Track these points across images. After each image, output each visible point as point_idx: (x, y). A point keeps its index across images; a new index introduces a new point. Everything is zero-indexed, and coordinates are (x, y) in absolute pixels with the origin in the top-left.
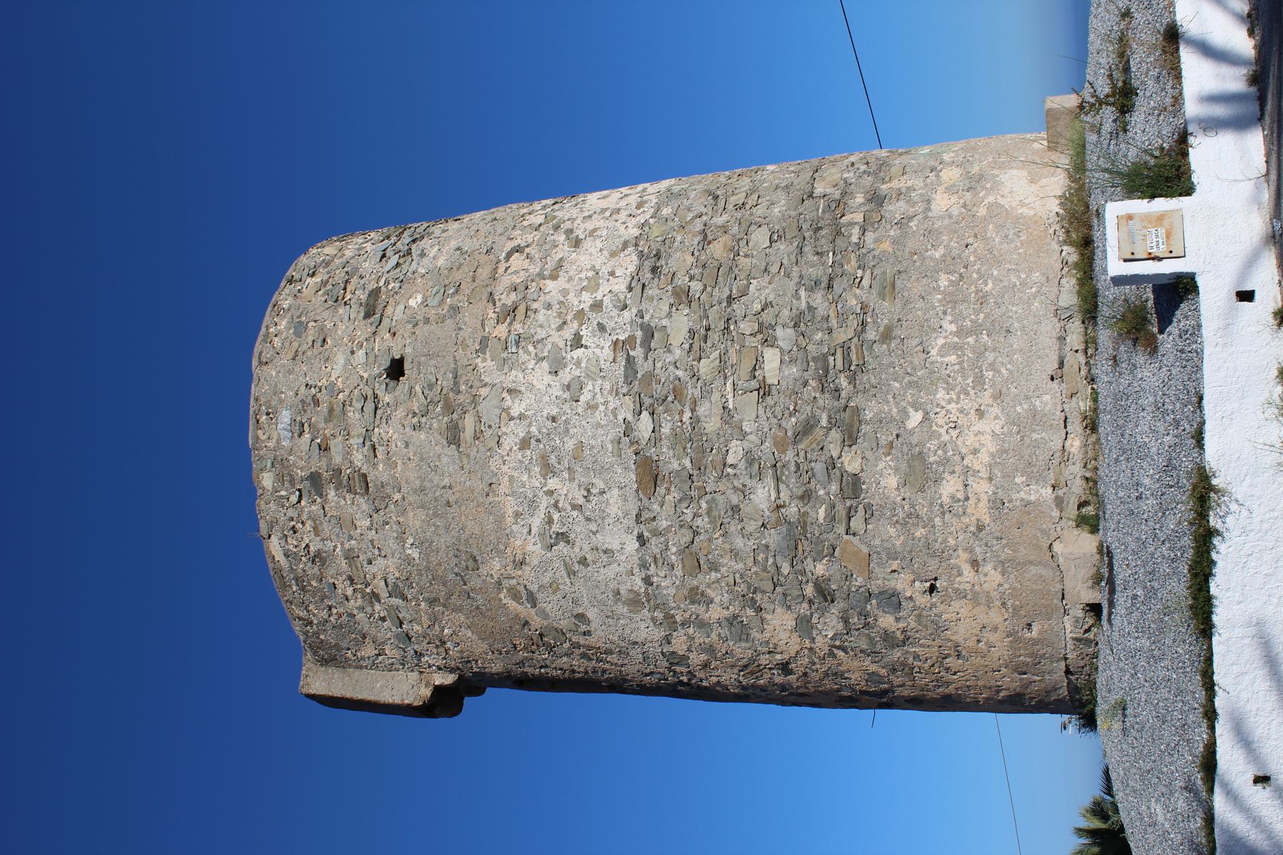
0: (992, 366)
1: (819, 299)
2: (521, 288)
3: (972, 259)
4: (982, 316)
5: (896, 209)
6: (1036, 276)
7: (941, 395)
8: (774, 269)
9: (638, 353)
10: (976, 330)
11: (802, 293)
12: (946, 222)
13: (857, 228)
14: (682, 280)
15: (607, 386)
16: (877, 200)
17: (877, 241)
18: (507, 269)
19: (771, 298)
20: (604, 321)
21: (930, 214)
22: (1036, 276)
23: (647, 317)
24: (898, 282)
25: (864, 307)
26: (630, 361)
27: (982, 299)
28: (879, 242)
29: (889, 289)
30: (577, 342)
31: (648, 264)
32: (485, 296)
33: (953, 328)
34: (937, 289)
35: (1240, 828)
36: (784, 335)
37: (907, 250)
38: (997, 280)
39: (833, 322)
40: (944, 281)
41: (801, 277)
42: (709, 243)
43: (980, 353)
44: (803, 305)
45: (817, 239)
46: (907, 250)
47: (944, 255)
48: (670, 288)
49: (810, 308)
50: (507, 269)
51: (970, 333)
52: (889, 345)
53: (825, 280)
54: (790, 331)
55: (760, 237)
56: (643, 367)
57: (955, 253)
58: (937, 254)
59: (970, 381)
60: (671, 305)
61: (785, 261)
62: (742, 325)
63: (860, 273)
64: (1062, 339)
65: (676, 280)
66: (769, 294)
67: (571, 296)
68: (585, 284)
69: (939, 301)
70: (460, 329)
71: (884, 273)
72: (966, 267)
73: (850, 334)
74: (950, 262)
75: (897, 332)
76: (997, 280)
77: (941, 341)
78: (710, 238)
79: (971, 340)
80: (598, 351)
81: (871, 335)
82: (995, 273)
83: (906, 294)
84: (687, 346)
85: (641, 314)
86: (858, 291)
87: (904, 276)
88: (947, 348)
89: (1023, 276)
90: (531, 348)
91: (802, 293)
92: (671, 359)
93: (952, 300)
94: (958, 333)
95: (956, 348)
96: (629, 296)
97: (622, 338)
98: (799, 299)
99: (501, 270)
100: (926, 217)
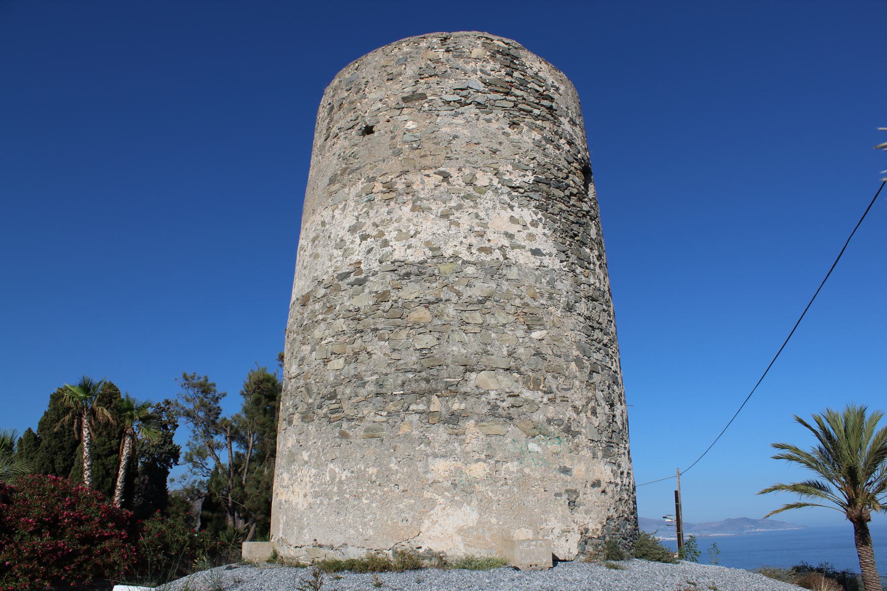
0: (322, 502)
1: (371, 388)
2: (409, 190)
3: (386, 489)
4: (348, 496)
5: (441, 433)
6: (371, 532)
7: (314, 471)
8: (395, 355)
9: (352, 278)
10: (341, 492)
11: (375, 377)
12: (421, 470)
13: (425, 408)
14: (394, 295)
15: (339, 264)
16: (454, 418)
17: (411, 422)
18: (428, 176)
19: (374, 357)
20: (374, 251)
21: (430, 458)
22: (371, 532)
23: (371, 278)
24: (374, 440)
25: (362, 419)
26: (348, 274)
27: (357, 497)
28: (411, 425)
29: (371, 434)
30: (364, 238)
31: (414, 269)
32: (406, 169)
33: (344, 478)
34: (367, 466)
35: (477, 556)
36: (351, 370)
37: (398, 444)
38: (369, 506)
39: (354, 400)
40: (372, 470)
41: (386, 374)
42: (427, 307)
43: (328, 495)
44: (366, 379)
45: (416, 381)
46: (398, 444)
47: (391, 470)
48: (390, 288)
49: (365, 383)
50: (428, 176)
51: (339, 488)
52: (338, 437)
53: (384, 391)
54: (352, 373)
55: (427, 340)
56: (343, 284)
57: (393, 478)
58: (393, 466)
59: (317, 489)
60: (376, 292)
61: (400, 362)
62: (360, 341)
63: (384, 413)
64: (332, 547)
65: (395, 291)
66: (378, 355)
67: (396, 225)
68: (404, 231)
69: (360, 468)
70: (384, 161)
71: (383, 430)
72: (380, 485)
73: (347, 412)
74: (386, 475)
75: (344, 441)
76: (369, 506)
77: (337, 470)
78: (431, 307)
79: (335, 489)
80: (357, 253)
81: (345, 425)
82: (374, 505)
83: (366, 446)
84: (351, 308)
85: (375, 274)
86: (372, 414)
87: (379, 443)
88: (333, 472)
89: (371, 523)
90: (364, 210)
91: (375, 377)
92: (346, 301)
93: (359, 476)
94: (341, 482)
95: (333, 478)
96: (389, 263)
97: (362, 266)
98: (372, 375)
99: (427, 172)
100: (428, 456)
